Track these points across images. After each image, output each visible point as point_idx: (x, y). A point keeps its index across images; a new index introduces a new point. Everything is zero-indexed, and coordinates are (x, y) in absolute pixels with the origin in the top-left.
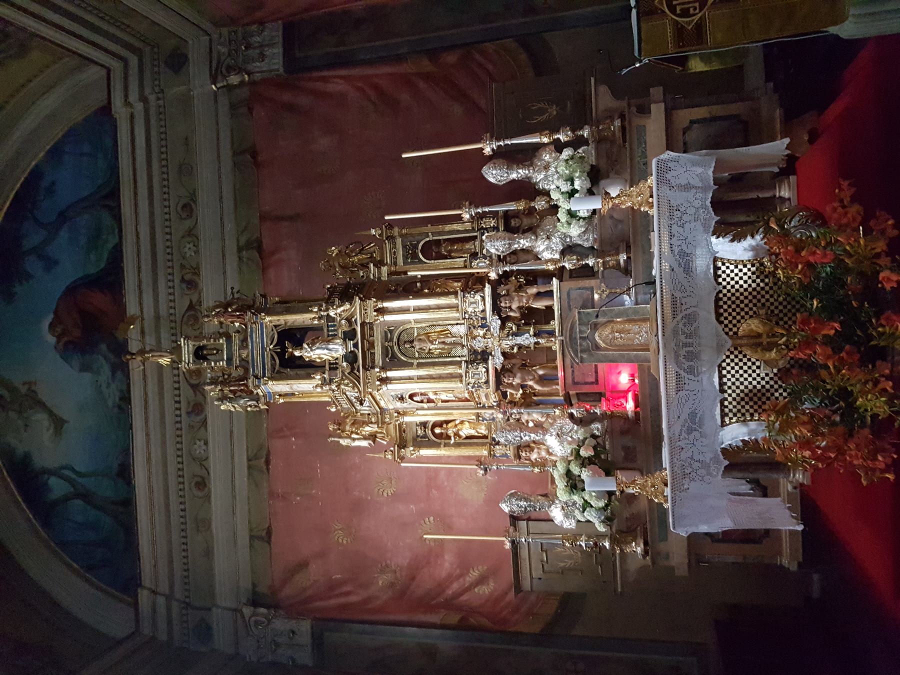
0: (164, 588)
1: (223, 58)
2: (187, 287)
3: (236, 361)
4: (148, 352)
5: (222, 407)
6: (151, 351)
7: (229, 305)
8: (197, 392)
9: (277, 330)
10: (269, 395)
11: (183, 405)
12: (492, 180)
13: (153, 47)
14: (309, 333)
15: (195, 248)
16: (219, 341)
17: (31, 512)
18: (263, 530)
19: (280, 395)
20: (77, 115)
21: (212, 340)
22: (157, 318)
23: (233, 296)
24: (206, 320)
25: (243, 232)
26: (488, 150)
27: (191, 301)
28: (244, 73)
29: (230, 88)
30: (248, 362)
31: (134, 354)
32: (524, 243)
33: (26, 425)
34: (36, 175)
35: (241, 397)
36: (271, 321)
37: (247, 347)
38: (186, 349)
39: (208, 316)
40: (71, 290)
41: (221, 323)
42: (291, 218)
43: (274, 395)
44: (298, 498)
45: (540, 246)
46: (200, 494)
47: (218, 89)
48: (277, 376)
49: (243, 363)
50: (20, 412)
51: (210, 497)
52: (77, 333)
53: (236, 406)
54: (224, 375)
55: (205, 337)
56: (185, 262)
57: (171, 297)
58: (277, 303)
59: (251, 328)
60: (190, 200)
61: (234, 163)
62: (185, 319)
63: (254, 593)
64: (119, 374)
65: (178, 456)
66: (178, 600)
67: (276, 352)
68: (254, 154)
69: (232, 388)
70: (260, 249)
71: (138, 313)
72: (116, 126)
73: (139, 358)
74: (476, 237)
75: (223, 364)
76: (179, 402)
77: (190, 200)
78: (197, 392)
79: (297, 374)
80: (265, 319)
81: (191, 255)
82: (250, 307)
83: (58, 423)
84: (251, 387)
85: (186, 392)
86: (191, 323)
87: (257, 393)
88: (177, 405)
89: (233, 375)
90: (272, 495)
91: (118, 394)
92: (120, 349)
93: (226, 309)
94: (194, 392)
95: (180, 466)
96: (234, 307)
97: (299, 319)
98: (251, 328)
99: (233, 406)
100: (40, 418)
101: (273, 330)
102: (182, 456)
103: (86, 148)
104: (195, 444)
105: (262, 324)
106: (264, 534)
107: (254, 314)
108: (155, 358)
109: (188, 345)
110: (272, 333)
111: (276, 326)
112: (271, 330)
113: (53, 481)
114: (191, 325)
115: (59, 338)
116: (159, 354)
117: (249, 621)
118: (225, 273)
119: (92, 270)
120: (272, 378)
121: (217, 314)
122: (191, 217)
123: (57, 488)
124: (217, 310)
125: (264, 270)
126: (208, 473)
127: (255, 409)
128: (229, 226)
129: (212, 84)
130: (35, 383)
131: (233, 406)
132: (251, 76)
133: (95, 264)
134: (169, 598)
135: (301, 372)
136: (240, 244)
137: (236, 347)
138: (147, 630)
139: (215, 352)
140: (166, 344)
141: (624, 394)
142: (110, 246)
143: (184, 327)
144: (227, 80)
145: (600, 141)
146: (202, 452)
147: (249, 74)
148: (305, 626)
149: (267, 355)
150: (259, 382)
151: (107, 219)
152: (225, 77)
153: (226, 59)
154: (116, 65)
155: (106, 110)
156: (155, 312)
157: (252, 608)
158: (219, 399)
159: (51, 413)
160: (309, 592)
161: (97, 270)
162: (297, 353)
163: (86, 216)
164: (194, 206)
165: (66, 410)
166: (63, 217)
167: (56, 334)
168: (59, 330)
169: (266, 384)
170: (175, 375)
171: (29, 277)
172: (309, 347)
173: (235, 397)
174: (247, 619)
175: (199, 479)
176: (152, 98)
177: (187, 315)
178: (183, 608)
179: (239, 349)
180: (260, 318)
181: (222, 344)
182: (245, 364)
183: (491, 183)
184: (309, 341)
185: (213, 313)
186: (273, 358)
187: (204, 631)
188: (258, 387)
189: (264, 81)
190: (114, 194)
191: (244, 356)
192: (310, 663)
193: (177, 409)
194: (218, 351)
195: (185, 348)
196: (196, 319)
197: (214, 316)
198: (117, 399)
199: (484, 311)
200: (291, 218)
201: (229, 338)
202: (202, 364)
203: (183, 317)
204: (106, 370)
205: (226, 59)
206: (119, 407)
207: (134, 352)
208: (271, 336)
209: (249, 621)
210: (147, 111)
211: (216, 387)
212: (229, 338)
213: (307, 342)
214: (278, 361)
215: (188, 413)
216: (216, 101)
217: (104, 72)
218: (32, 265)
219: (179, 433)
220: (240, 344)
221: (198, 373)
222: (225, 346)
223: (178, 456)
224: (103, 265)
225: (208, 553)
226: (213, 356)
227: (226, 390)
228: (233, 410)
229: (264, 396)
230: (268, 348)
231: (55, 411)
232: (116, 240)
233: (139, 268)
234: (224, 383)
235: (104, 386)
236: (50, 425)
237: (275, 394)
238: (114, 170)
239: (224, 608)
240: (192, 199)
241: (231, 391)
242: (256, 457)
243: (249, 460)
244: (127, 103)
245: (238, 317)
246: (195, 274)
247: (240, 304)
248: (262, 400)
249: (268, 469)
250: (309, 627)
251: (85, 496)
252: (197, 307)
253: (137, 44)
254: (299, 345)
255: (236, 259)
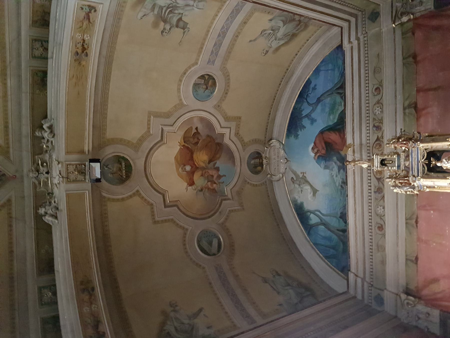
0: (361, 274)
1: (399, 9)
2: (376, 130)
3: (402, 167)
4: (356, 161)
5: (395, 191)
6: (358, 161)
7: (399, 138)
8: (380, 182)
9: (426, 152)
10: (420, 186)
11: (373, 188)
13: (362, 12)
14: (444, 154)
15: (381, 110)
16: (393, 156)
17: (303, 228)
18: (414, 257)
19: (427, 187)
20: (327, 52)
21: (390, 156)
22: (361, 144)
23: (402, 133)
24: (388, 146)
25: (407, 99)
27: (378, 137)
28: (410, 15)
29: (402, 24)
30: (409, 168)
31: (350, 162)
33: (302, 191)
34: (308, 82)
35: (405, 186)
36: (423, 147)
37: (409, 160)
38: (376, 160)
39: (389, 144)
41: (395, 147)
42: (435, 89)
43: (424, 187)
44: (434, 244)
46: (380, 233)
47: (396, 26)
48: (426, 176)
49: (406, 168)
50: (300, 185)
51: (385, 235)
52: (323, 152)
53: (402, 190)
54: (396, 174)
55: (385, 155)
56: (375, 117)
57: (368, 135)
58: (427, 136)
59: (412, 151)
60: (379, 85)
61: (404, 64)
62: (374, 145)
63: (407, 288)
64: (342, 171)
65: (369, 213)
66: (367, 282)
67: (425, 164)
69: (400, 181)
70: (416, 108)
71: (352, 143)
72: (344, 55)
73: (353, 164)
75: (395, 168)
76: (371, 186)
77: (379, 85)
78: (380, 182)
79: (438, 176)
80: (420, 145)
81: (378, 113)
82: (411, 139)
83: (315, 191)
84: (411, 181)
85: (374, 181)
86: (377, 147)
87: (414, 185)
88: (370, 188)
89: (401, 174)
90: (419, 239)
91: (341, 180)
92: (343, 160)
93: (398, 141)
94: (379, 182)
95: (370, 217)
96: (402, 139)
97: (440, 145)
98: (412, 151)
99: (401, 191)
101: (424, 151)
102: (371, 213)
104: (378, 208)
105: (418, 148)
106: (414, 259)
107: (413, 142)
108: (360, 164)
109: (377, 158)
110: (423, 153)
111: (426, 149)
112: (423, 151)
113: (312, 216)
114: (378, 148)
115: (316, 154)
116: (362, 162)
117: (404, 302)
118: (396, 121)
119: (331, 123)
120: (423, 177)
121: (394, 143)
122: (379, 94)
123: (314, 219)
124: (394, 141)
125: (418, 119)
126: (385, 223)
127: (412, 193)
128: (399, 97)
129: (393, 24)
130: (306, 173)
131: (401, 191)
132: (414, 15)
133: (333, 120)
134: (363, 280)
135: (440, 175)
136: (405, 106)
137: (402, 160)
138: (352, 292)
139: (391, 162)
140: (364, 157)
142: (339, 112)
143: (374, 149)
144: (401, 20)
146: (382, 212)
147: (413, 14)
148: (436, 313)
149: (420, 165)
150: (416, 179)
151: (338, 99)
152: (400, 19)
153: (400, 9)
154: (345, 25)
155: (340, 47)
156: (360, 142)
157: (406, 296)
158: (393, 186)
159: (311, 186)
160: (439, 296)
161: (333, 123)
162: (439, 164)
163: (329, 99)
164: (381, 89)
165: (318, 185)
167: (315, 152)
168: (316, 150)
169: (419, 180)
170: (369, 173)
172: (446, 161)
173: (402, 185)
174: (403, 301)
175: (380, 225)
176: (361, 37)
177: (376, 143)
178: (370, 286)
179: (404, 161)
180: (417, 145)
181: (395, 158)
182: (407, 169)
184: (447, 158)
185: (391, 142)
186: (423, 166)
187: (380, 300)
188: (415, 181)
189: (423, 17)
190: (342, 87)
191: (407, 165)
192: (438, 334)
193: (369, 189)
194: (392, 162)
195: (376, 160)
196: (380, 146)
197: (392, 144)
198: (340, 183)
200: (435, 89)
201: (399, 155)
202: (384, 168)
203: (374, 145)
204: (336, 169)
205: (400, 9)
206: (342, 186)
207: (349, 161)
208: (423, 155)
209: (404, 302)
210: (359, 44)
211: (392, 180)
212: (399, 155)
213: (445, 158)
214: (426, 168)
215: (375, 192)
216: (394, 32)
217: (340, 29)
219: (370, 201)
220: (405, 158)
221: (380, 172)
222: (396, 159)
223: (369, 213)
224: (336, 121)
225: (383, 262)
226: (390, 164)
227: (397, 182)
228: (400, 192)
229: (417, 187)
230: (421, 161)
231: (314, 186)
232: (343, 108)
233: (353, 120)
234: (396, 178)
235: (335, 176)
236: (311, 191)
237: (424, 186)
238: (343, 75)
239: (390, 292)
240: (380, 85)
241: (399, 182)
242: (410, 218)
243: (406, 219)
244: (350, 42)
245: (405, 144)
246: (380, 123)
247: (406, 137)
248: (417, 188)
249: (417, 226)
250: (438, 314)
252: (381, 140)
253: (353, 11)
254: (439, 159)
255: (403, 114)
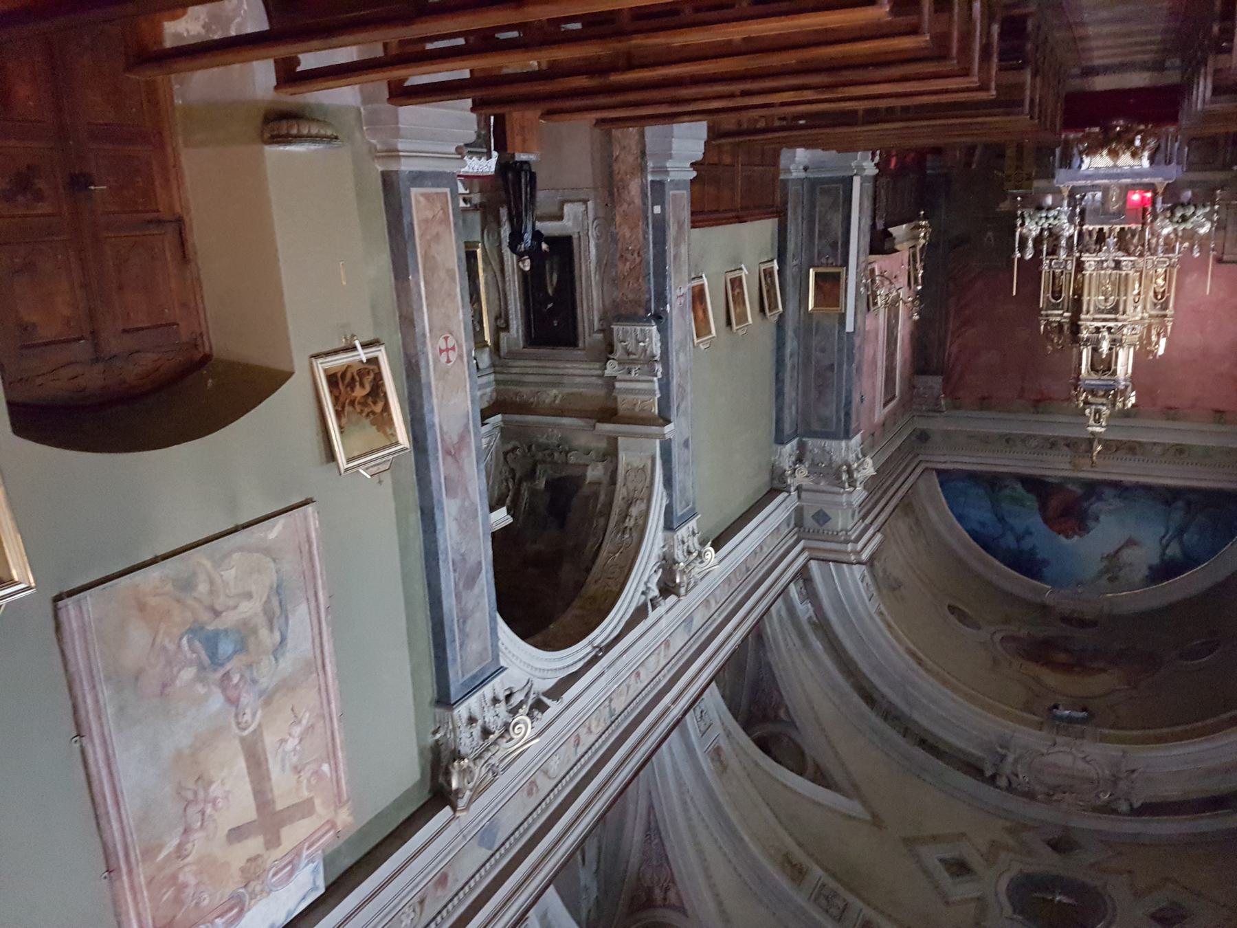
12: (1030, 256)
26: (1018, 255)
32: (1063, 243)
40: (1046, 521)
45: (1067, 234)
50: (1120, 569)
68: (984, 398)
70: (1039, 401)
74: (1054, 272)
83: (1130, 543)
100: (1128, 555)
103: (962, 499)
113: (1169, 552)
115: (1075, 533)
119: (1036, 505)
123: (1174, 550)
141: (1143, 198)
145: (1023, 207)
166: (1001, 520)
168: (1070, 533)
171: (1034, 547)
183: (1031, 259)
199: (1095, 261)
218: (1027, 544)
235: (1111, 508)
243: (1168, 419)
251: (1181, 531)
